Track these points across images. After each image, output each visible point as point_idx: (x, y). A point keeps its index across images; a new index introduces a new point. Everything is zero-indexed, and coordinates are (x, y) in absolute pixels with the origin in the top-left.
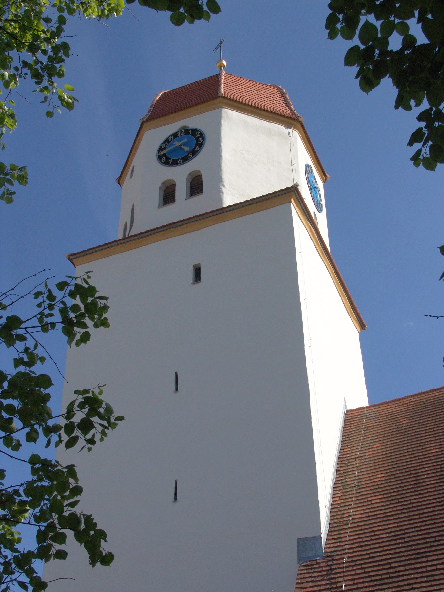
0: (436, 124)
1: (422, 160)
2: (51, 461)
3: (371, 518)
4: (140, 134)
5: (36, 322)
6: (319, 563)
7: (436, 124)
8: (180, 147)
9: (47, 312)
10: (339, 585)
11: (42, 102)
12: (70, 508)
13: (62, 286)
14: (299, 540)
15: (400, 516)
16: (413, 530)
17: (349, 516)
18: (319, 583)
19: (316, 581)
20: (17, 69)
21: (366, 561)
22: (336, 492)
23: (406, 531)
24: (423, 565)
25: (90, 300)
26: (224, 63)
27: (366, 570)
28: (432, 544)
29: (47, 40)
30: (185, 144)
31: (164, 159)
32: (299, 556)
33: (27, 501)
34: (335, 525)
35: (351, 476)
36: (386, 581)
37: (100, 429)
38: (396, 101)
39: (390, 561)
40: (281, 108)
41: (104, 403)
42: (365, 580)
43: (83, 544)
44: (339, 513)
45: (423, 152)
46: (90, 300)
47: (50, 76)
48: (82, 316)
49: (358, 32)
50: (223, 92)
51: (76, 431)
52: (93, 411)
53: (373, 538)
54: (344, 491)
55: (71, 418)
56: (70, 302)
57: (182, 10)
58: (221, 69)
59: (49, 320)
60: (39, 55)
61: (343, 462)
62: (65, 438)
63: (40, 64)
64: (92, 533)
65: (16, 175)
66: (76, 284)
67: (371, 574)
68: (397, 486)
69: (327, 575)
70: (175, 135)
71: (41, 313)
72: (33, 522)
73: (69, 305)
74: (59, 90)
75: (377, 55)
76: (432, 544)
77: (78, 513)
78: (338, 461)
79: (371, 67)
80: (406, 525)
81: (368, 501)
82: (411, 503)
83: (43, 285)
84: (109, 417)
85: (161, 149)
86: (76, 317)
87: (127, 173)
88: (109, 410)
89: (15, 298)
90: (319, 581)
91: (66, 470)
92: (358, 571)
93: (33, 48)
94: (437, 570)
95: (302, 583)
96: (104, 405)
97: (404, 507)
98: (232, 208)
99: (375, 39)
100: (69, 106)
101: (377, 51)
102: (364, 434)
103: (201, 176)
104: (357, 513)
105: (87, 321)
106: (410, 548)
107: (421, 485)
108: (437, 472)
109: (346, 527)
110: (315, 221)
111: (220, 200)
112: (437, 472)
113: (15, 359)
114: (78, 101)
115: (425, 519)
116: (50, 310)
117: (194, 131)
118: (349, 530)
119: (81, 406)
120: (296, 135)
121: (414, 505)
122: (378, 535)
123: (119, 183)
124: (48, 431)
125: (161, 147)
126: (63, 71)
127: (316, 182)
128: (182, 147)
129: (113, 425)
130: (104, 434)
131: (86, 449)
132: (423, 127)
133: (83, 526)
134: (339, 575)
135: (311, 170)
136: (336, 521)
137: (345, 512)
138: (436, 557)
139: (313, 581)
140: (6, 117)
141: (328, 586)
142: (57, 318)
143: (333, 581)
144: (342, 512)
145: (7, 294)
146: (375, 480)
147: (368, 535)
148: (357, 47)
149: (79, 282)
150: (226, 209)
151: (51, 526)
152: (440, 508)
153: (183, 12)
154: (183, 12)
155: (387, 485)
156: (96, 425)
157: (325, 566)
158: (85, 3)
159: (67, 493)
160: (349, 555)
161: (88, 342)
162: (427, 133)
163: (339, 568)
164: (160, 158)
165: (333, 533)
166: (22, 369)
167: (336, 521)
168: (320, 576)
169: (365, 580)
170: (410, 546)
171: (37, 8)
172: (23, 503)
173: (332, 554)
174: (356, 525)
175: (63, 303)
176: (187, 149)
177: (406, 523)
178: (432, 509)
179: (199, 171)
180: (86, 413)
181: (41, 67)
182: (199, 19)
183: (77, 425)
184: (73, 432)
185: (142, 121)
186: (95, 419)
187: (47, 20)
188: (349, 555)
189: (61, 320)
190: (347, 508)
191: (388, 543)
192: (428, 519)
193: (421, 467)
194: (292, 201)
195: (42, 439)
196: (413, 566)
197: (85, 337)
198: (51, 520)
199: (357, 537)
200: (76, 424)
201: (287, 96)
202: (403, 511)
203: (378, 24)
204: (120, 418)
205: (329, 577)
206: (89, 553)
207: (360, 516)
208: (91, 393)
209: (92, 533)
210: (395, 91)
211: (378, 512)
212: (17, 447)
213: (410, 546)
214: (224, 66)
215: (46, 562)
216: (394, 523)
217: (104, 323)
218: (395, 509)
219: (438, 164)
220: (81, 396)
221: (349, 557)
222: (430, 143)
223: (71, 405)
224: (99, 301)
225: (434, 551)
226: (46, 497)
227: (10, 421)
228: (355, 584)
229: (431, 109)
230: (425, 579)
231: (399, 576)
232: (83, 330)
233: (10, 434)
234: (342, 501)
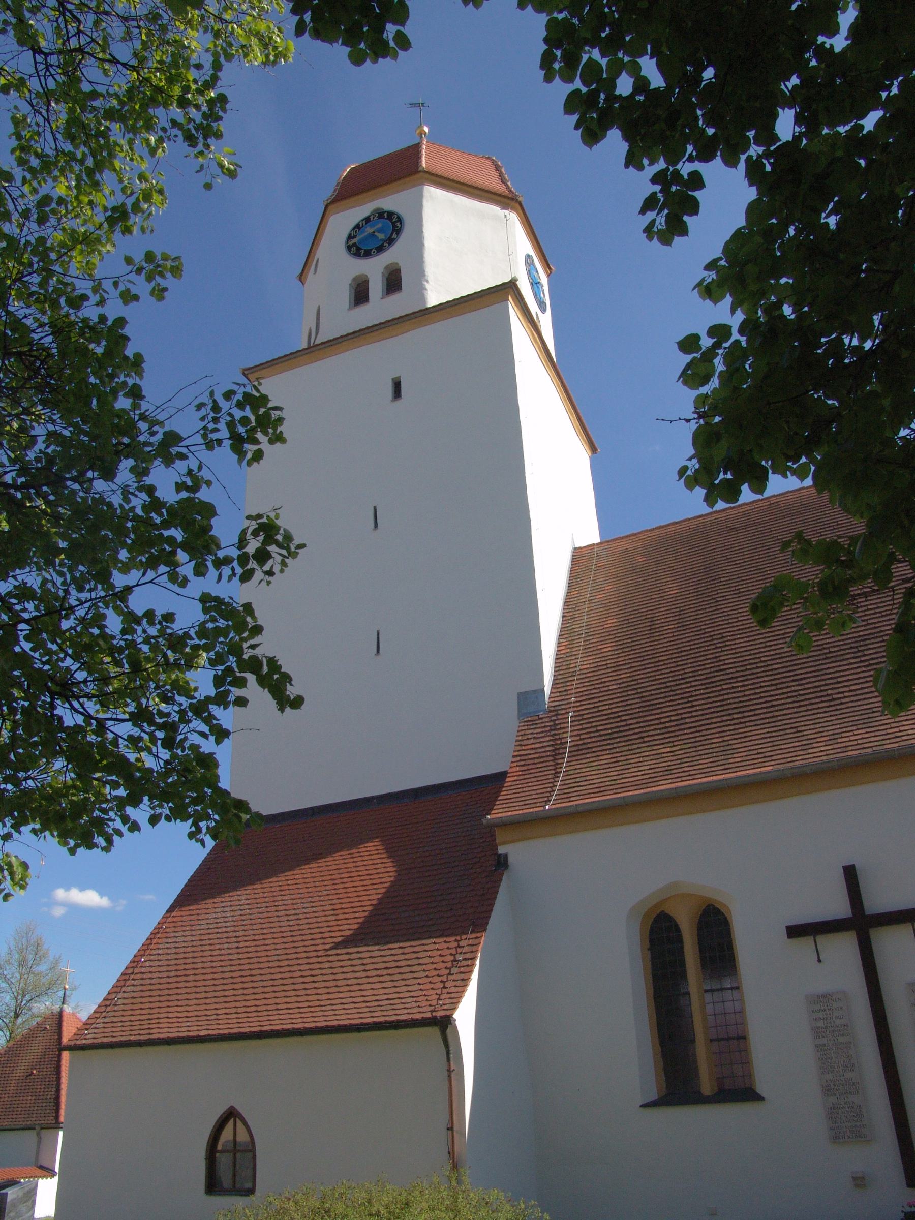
0: (674, 188)
1: (657, 233)
2: (224, 599)
3: (600, 668)
4: (324, 220)
5: (198, 439)
6: (542, 718)
7: (674, 188)
8: (372, 235)
9: (211, 426)
10: (563, 741)
11: (197, 172)
12: (250, 650)
13: (228, 395)
14: (520, 695)
15: (633, 665)
16: (647, 680)
17: (576, 667)
18: (542, 740)
19: (538, 738)
20: (164, 130)
21: (594, 715)
22: (561, 641)
23: (640, 681)
24: (657, 716)
25: (262, 411)
26: (426, 129)
27: (594, 724)
28: (667, 694)
29: (200, 92)
30: (380, 231)
31: (353, 249)
32: (519, 711)
33: (199, 644)
34: (559, 677)
35: (579, 622)
36: (615, 735)
37: (279, 558)
38: (626, 158)
39: (620, 714)
40: (495, 184)
41: (282, 529)
42: (592, 735)
43: (266, 690)
44: (564, 663)
45: (657, 223)
46: (262, 411)
47: (206, 138)
48: (253, 430)
49: (579, 73)
50: (424, 166)
51: (251, 562)
52: (270, 539)
53: (602, 690)
54: (570, 639)
55: (244, 547)
56: (238, 414)
57: (362, 46)
58: (421, 137)
59: (214, 436)
60: (193, 112)
61: (570, 607)
62: (239, 571)
63: (192, 123)
64: (276, 676)
65: (169, 267)
66: (244, 393)
67: (599, 728)
68: (631, 632)
69: (551, 730)
70: (367, 220)
71: (205, 428)
72: (207, 666)
73: (237, 417)
74: (216, 155)
75: (602, 101)
76: (667, 694)
77: (259, 656)
78: (564, 606)
79: (595, 116)
80: (639, 674)
81: (597, 650)
82: (645, 651)
83: (207, 394)
84: (288, 545)
85: (350, 237)
86: (246, 431)
87: (310, 266)
88: (288, 537)
89: (172, 411)
90: (542, 737)
91: (242, 609)
92: (585, 726)
93: (183, 103)
94: (671, 721)
95: (523, 740)
96: (281, 531)
97: (637, 655)
98: (437, 308)
99: (600, 80)
100: (232, 174)
101: (602, 96)
102: (594, 574)
103: (400, 270)
104: (585, 663)
105: (259, 436)
106: (643, 700)
107: (657, 630)
108: (676, 616)
109: (572, 678)
110: (538, 324)
111: (423, 299)
112: (676, 616)
113: (177, 483)
114: (241, 167)
115: (660, 668)
116: (215, 424)
117: (391, 215)
118: (576, 682)
119: (255, 533)
120: (514, 218)
121: (649, 653)
122: (608, 686)
123: (301, 280)
124: (220, 563)
125: (350, 234)
126: (221, 132)
127: (539, 276)
128: (376, 234)
129: (293, 555)
130: (284, 564)
131: (264, 583)
132: (658, 191)
133: (265, 669)
134: (563, 731)
135: (533, 261)
136: (561, 672)
137: (572, 662)
138: (671, 708)
139: (534, 738)
140: (154, 193)
141: (552, 743)
142: (224, 433)
143: (557, 737)
144: (568, 663)
145: (163, 407)
146: (605, 626)
147: (597, 686)
148: (578, 91)
149: (248, 389)
150: (432, 309)
151: (229, 670)
152: (677, 655)
153: (364, 48)
154: (364, 48)
155: (619, 631)
156: (274, 555)
157: (547, 722)
158: (245, 45)
159: (246, 635)
160: (576, 709)
161: (261, 461)
162: (662, 199)
163: (564, 723)
164: (349, 248)
165: (558, 686)
166: (184, 494)
167: (561, 672)
168: (543, 732)
169: (592, 735)
170: (642, 697)
171: (186, 54)
172: (196, 648)
173: (557, 708)
174: (584, 676)
175: (230, 415)
176: (381, 236)
177: (639, 672)
178: (668, 657)
179: (397, 264)
180: (261, 541)
181: (194, 127)
182: (384, 57)
183: (252, 556)
184: (247, 564)
185: (326, 203)
186: (273, 548)
187: (199, 67)
188: (576, 709)
189: (228, 436)
190: (574, 657)
191: (618, 695)
192: (663, 667)
193: (657, 611)
194: (510, 298)
195: (212, 573)
196: (645, 719)
197: (258, 456)
198: (229, 664)
199: (585, 689)
200: (251, 554)
201: (503, 170)
202: (636, 660)
203: (604, 62)
204: (301, 546)
205: (552, 733)
206: (274, 698)
207: (588, 666)
208: (265, 517)
209: (276, 676)
210: (624, 147)
211: (608, 662)
212: (184, 583)
213: (642, 697)
214: (425, 133)
215: (225, 709)
216: (626, 673)
217: (278, 438)
218: (627, 658)
219: (675, 237)
220: (254, 522)
221: (574, 711)
222: (666, 211)
223: (244, 532)
224: (272, 412)
225: (669, 701)
226: (221, 639)
227: (174, 553)
228: (581, 739)
229: (667, 169)
230: (658, 732)
231: (630, 730)
232: (255, 447)
233: (174, 569)
234: (568, 650)
